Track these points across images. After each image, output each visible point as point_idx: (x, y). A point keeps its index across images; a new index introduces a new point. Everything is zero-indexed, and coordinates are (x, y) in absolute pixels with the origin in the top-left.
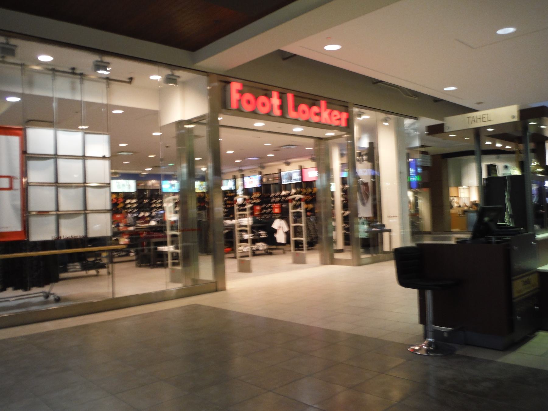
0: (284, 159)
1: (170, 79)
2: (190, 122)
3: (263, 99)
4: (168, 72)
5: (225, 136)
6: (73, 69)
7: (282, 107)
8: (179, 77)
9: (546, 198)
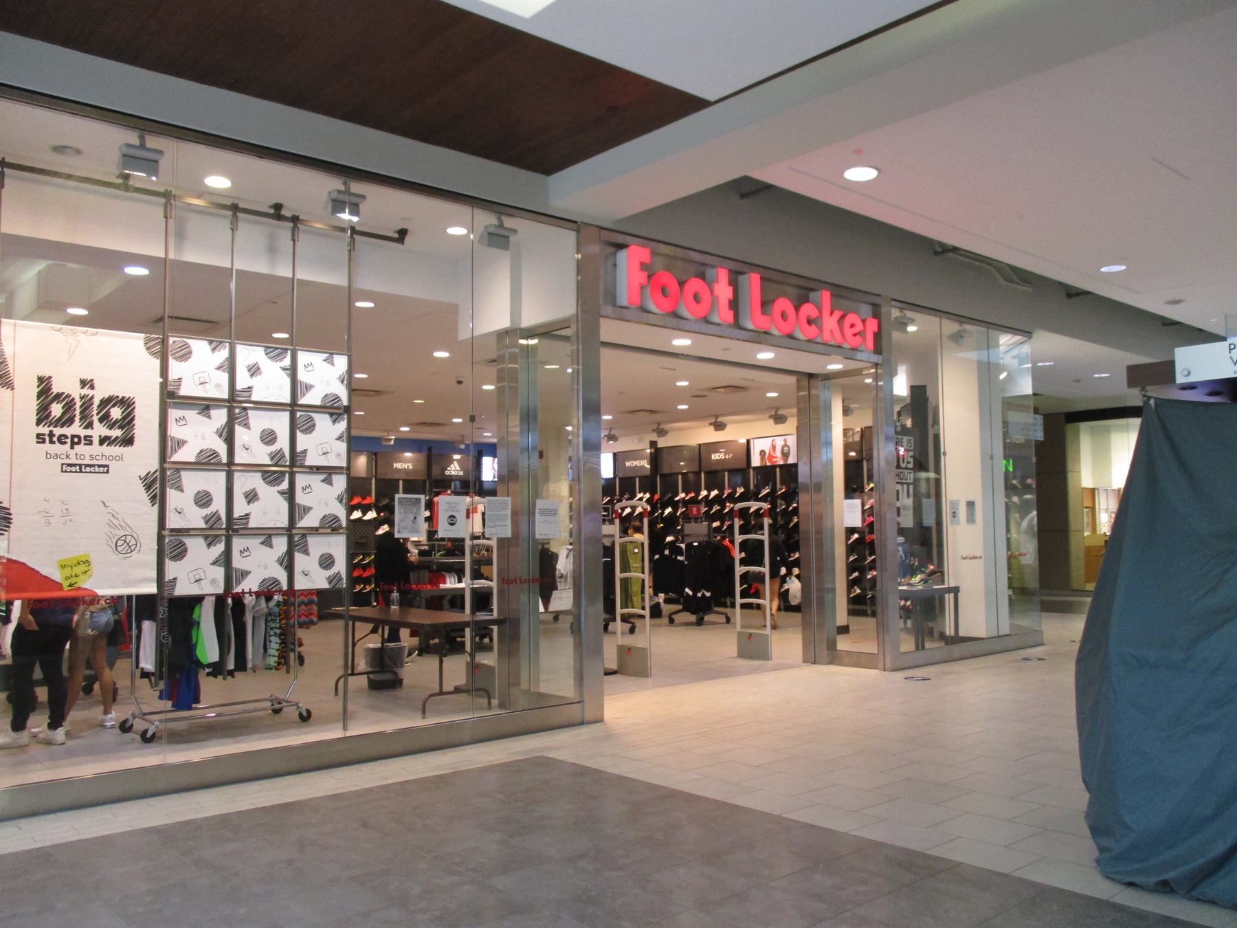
0: (712, 416)
1: (498, 239)
2: (529, 333)
3: (694, 285)
4: (486, 219)
5: (612, 365)
6: (278, 207)
7: (734, 304)
8: (515, 231)
9: (373, 625)
